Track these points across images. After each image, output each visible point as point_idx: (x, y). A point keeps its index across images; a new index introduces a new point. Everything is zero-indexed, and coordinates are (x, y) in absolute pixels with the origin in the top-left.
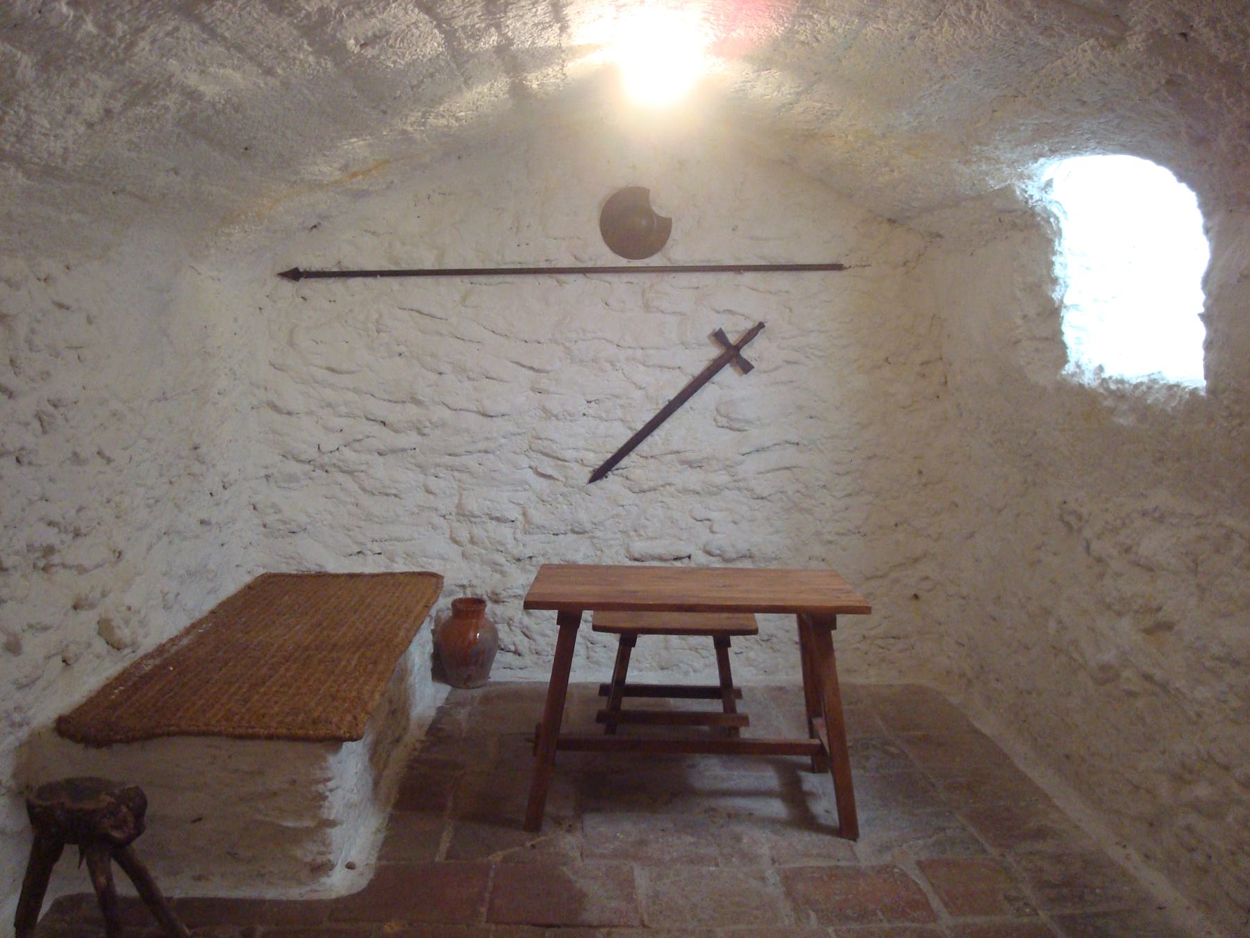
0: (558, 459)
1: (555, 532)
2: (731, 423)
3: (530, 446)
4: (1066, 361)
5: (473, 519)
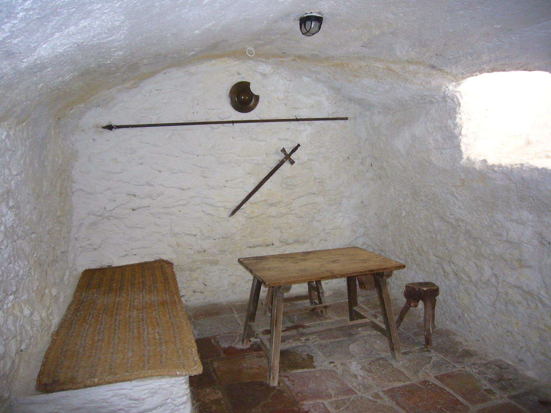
0: (215, 206)
1: (215, 238)
2: (288, 186)
3: (202, 202)
4: (462, 158)
5: (178, 236)
